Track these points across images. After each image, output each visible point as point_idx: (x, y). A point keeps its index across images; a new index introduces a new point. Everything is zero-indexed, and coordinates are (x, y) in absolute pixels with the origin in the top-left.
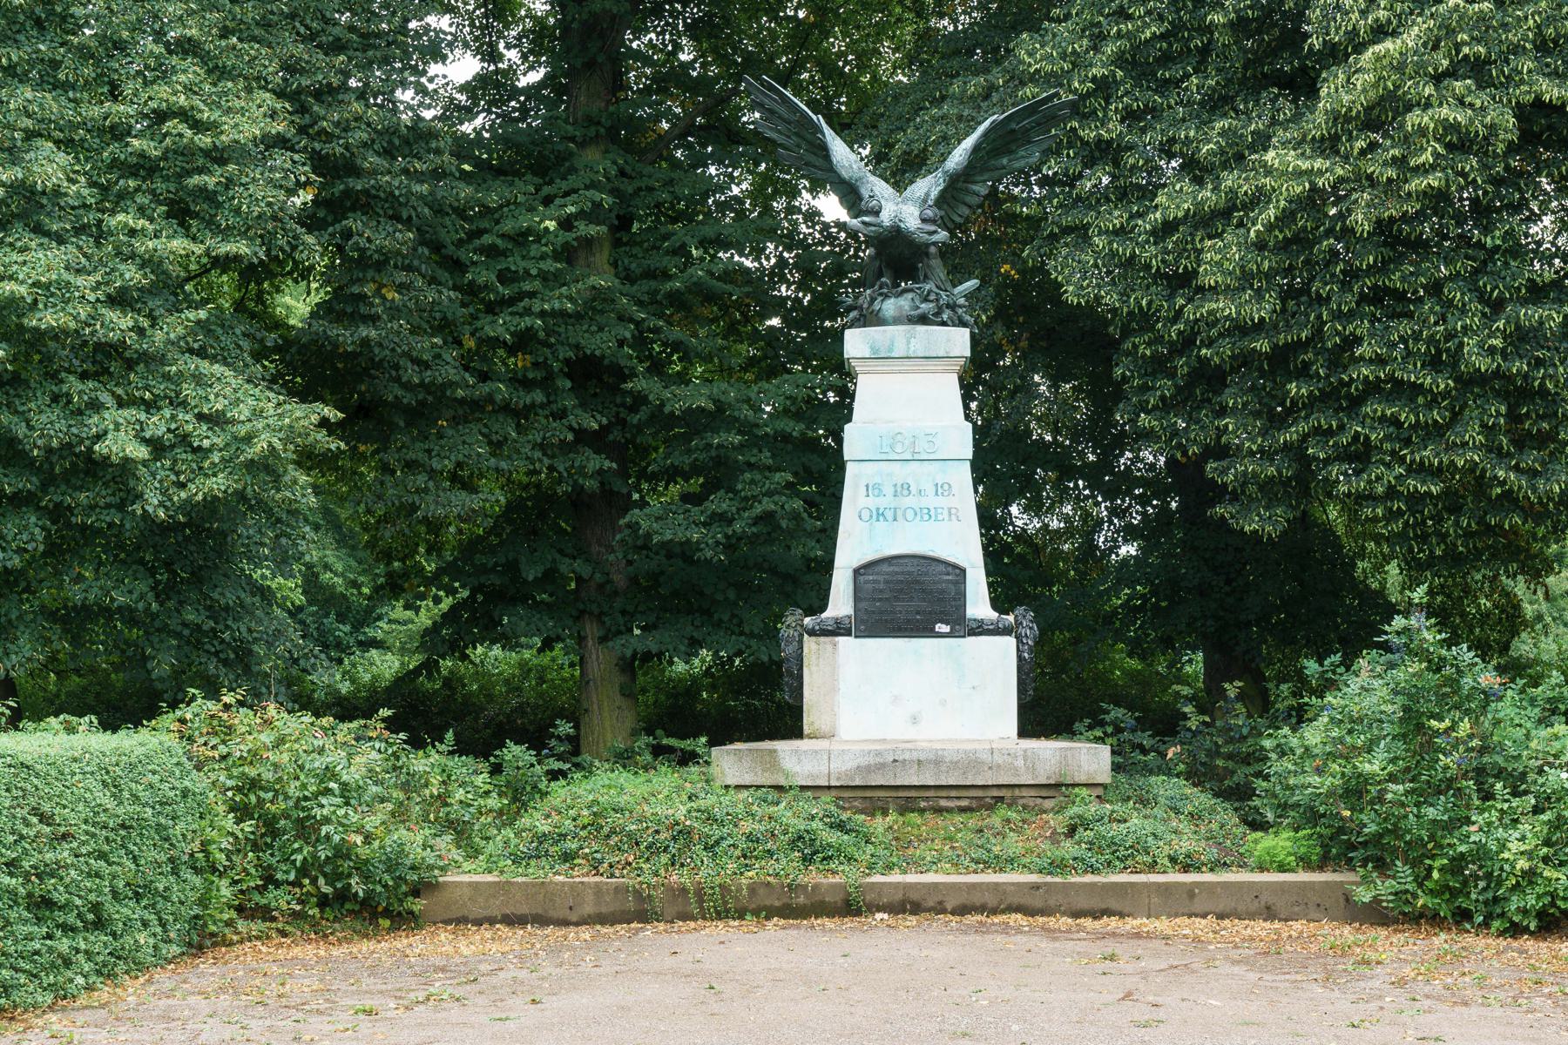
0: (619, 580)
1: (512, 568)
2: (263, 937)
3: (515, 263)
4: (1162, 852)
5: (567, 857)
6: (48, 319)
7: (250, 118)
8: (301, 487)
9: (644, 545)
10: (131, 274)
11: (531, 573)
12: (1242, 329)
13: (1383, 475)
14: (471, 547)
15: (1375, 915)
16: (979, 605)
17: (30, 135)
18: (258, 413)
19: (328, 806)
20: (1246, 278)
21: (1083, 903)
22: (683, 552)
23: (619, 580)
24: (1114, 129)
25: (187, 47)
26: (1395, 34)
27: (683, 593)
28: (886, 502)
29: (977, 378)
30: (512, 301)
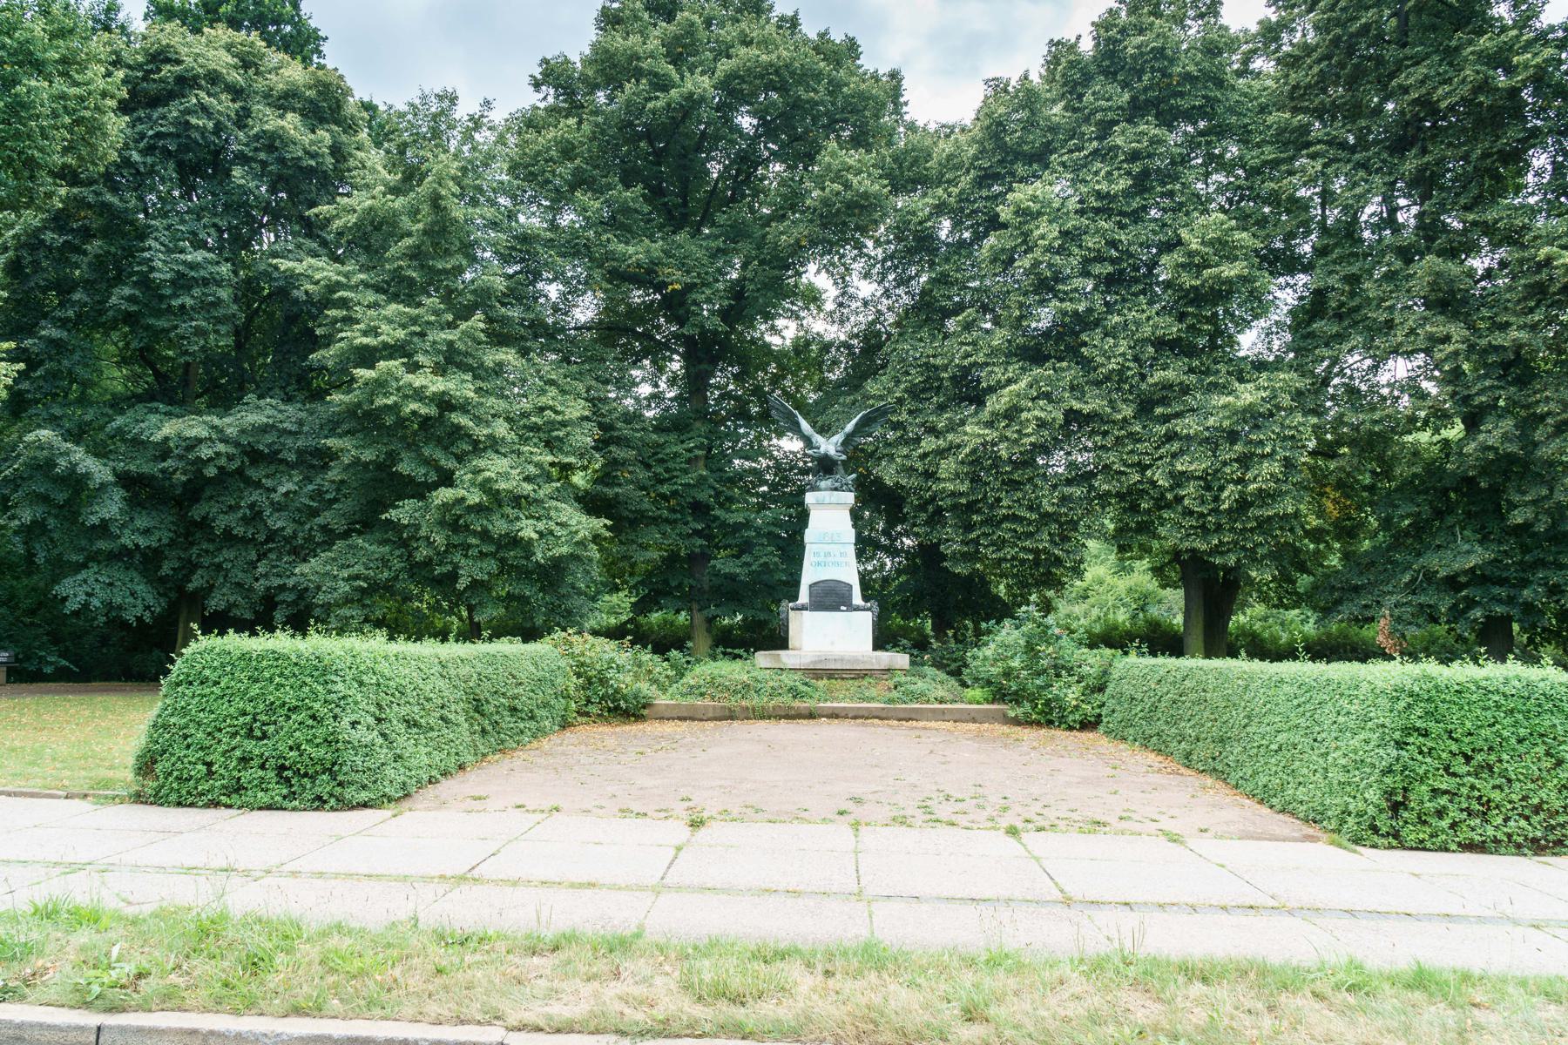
0: (706, 587)
1: (666, 582)
2: (498, 722)
3: (670, 465)
4: (932, 696)
5: (702, 694)
6: (502, 485)
7: (576, 409)
8: (594, 552)
9: (717, 574)
10: (532, 470)
11: (673, 584)
12: (953, 494)
13: (1009, 552)
14: (649, 574)
15: (1016, 722)
16: (857, 599)
17: (494, 416)
18: (579, 523)
19: (611, 674)
20: (957, 475)
21: (902, 715)
22: (732, 577)
23: (706, 587)
24: (904, 416)
25: (552, 383)
26: (1016, 382)
27: (731, 592)
28: (821, 559)
29: (856, 515)
30: (670, 479)
